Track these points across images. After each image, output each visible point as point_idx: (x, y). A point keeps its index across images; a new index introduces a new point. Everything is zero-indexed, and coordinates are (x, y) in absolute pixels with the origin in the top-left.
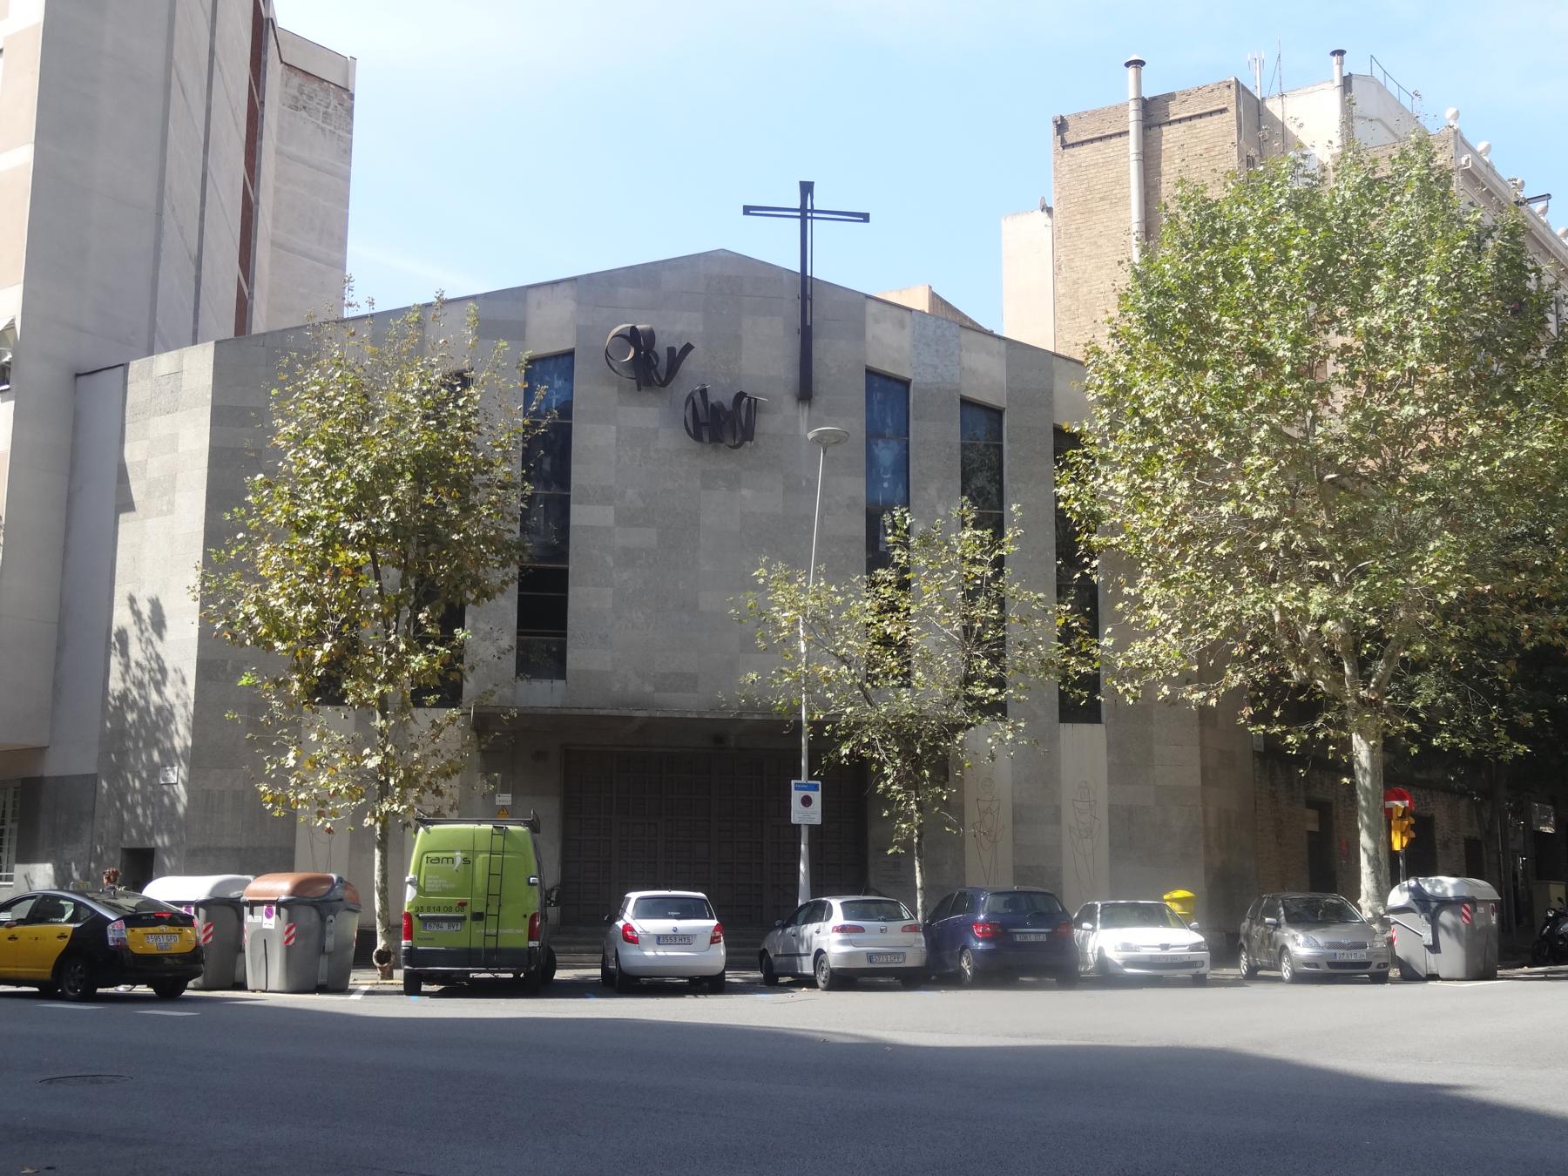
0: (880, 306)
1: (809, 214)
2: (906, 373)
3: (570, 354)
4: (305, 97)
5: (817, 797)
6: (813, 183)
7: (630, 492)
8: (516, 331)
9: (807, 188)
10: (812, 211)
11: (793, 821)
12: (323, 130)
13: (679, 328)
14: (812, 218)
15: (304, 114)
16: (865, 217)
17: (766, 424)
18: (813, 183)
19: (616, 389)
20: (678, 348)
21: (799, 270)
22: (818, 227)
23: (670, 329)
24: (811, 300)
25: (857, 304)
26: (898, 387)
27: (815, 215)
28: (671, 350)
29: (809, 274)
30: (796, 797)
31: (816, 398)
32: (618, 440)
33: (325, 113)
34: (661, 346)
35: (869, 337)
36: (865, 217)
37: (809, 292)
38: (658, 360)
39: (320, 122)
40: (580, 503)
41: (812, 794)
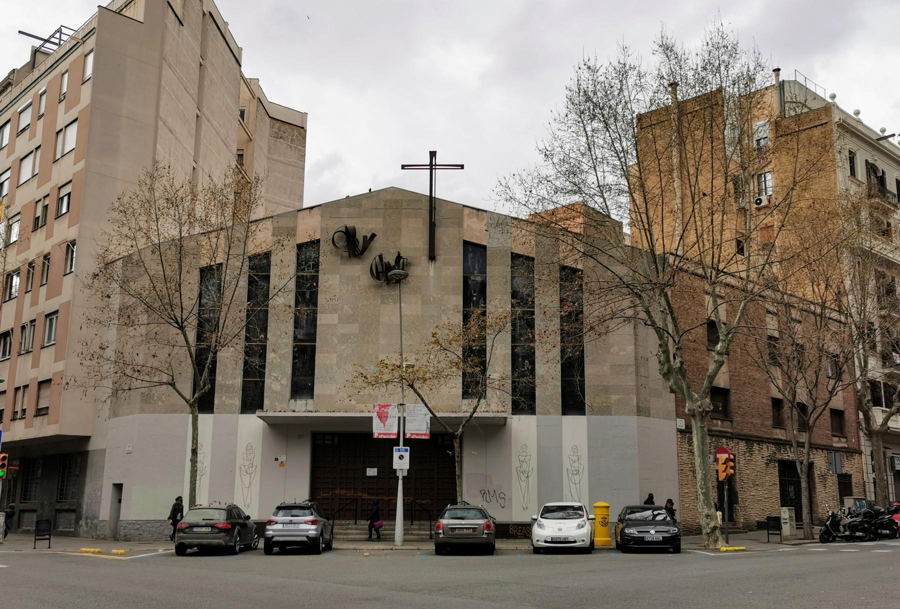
0: (471, 210)
1: (434, 167)
2: (485, 243)
3: (318, 241)
4: (281, 132)
5: (407, 455)
6: (430, 152)
7: (346, 307)
8: (291, 232)
9: (433, 154)
10: (435, 165)
11: (394, 468)
12: (291, 147)
13: (371, 226)
14: (435, 169)
15: (281, 140)
16: (462, 167)
17: (415, 272)
18: (430, 152)
19: (340, 257)
20: (369, 236)
21: (429, 195)
22: (438, 173)
23: (363, 229)
24: (435, 208)
25: (459, 211)
26: (482, 250)
27: (437, 167)
28: (365, 237)
29: (433, 196)
30: (396, 455)
31: (438, 257)
32: (340, 281)
33: (292, 139)
34: (360, 237)
35: (465, 226)
36: (462, 167)
37: (433, 206)
38: (358, 243)
39: (289, 143)
40: (322, 313)
41: (404, 454)
